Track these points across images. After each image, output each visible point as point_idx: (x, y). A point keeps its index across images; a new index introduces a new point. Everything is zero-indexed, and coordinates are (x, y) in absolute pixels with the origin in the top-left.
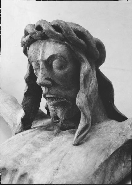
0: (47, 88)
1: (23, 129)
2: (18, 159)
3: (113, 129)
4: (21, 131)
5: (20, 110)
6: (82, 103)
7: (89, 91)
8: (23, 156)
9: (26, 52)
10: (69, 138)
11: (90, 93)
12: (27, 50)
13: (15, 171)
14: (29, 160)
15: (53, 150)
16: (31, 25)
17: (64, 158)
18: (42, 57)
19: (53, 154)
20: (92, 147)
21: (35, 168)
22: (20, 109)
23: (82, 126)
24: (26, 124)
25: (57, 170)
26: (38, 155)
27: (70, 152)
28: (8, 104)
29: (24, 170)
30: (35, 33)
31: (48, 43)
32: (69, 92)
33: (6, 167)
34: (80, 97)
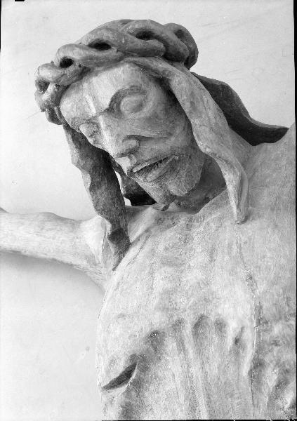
0: (132, 155)
1: (121, 252)
2: (167, 302)
3: (277, 159)
4: (119, 261)
5: (81, 227)
6: (212, 143)
7: (209, 117)
8: (168, 294)
9: (55, 117)
10: (220, 219)
11: (213, 121)
12: (57, 113)
13: (178, 325)
14: (187, 293)
15: (212, 253)
16: (46, 65)
17: (244, 255)
18: (97, 108)
19: (219, 258)
20: (272, 210)
21: (211, 299)
22: (79, 226)
23: (234, 182)
24: (119, 238)
25: (251, 278)
26: (193, 276)
27: (244, 239)
28: (51, 230)
29: (194, 314)
30: (62, 76)
31: (94, 80)
32: (173, 139)
33: (156, 327)
34: (201, 137)
